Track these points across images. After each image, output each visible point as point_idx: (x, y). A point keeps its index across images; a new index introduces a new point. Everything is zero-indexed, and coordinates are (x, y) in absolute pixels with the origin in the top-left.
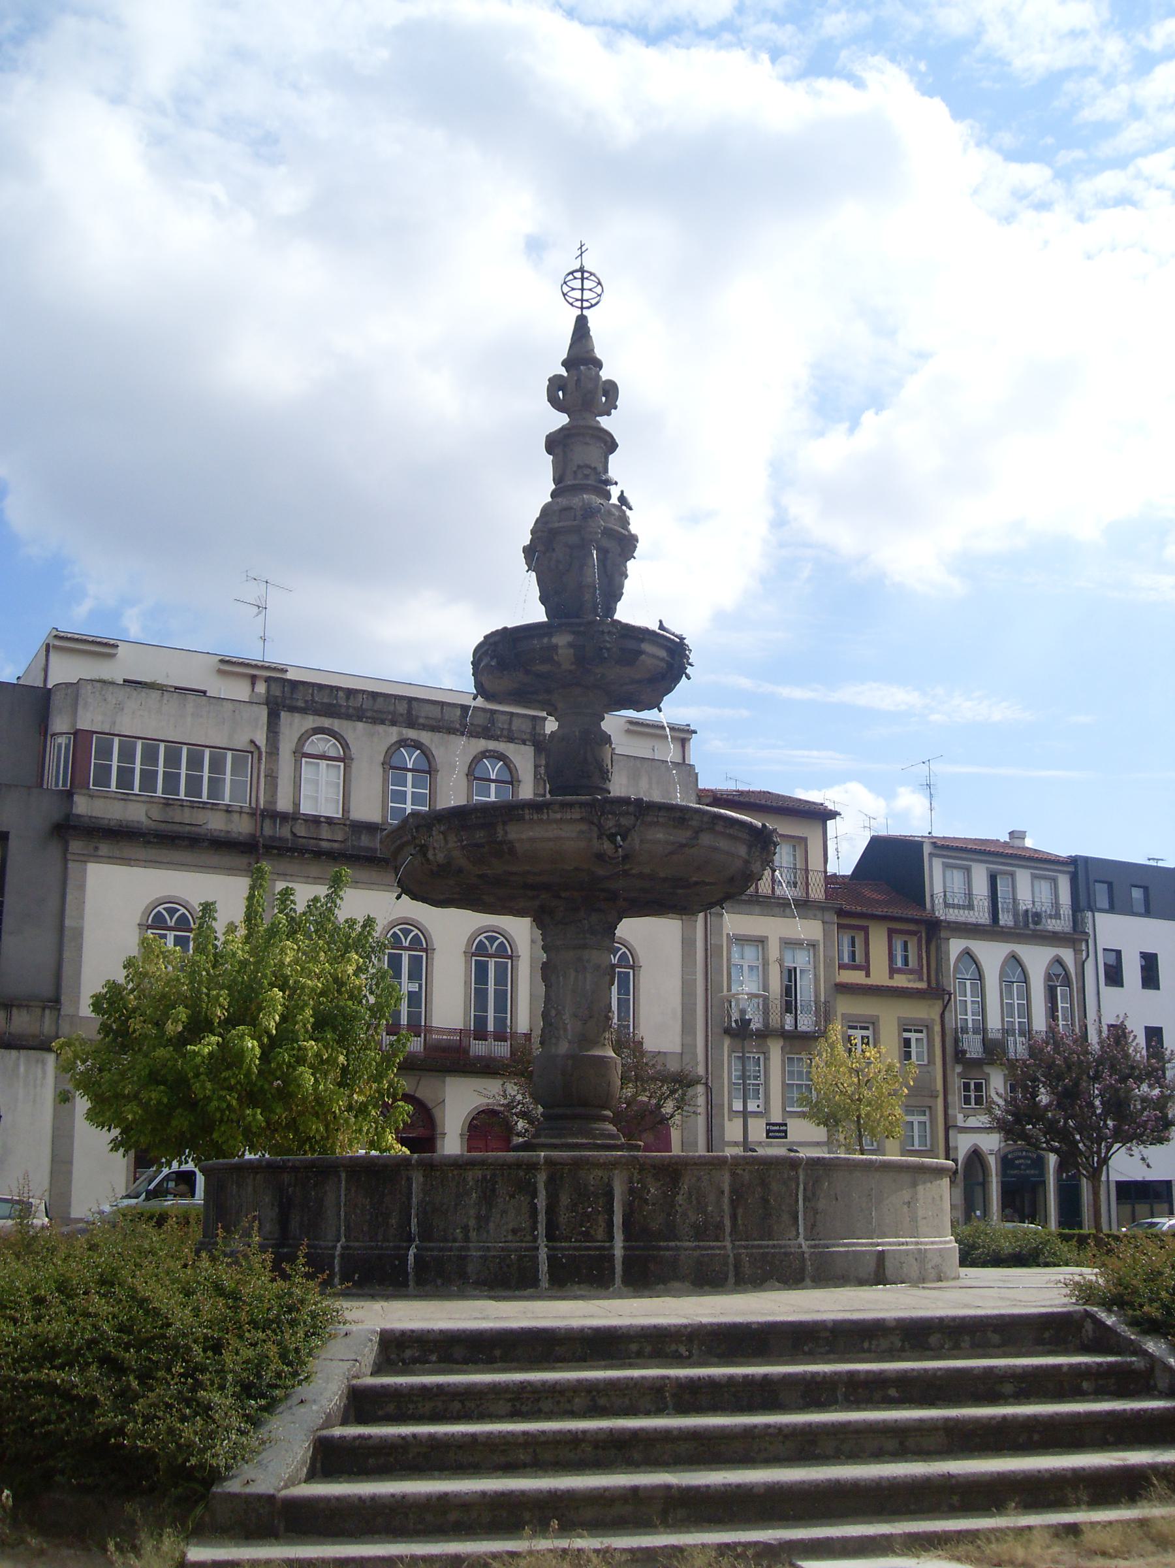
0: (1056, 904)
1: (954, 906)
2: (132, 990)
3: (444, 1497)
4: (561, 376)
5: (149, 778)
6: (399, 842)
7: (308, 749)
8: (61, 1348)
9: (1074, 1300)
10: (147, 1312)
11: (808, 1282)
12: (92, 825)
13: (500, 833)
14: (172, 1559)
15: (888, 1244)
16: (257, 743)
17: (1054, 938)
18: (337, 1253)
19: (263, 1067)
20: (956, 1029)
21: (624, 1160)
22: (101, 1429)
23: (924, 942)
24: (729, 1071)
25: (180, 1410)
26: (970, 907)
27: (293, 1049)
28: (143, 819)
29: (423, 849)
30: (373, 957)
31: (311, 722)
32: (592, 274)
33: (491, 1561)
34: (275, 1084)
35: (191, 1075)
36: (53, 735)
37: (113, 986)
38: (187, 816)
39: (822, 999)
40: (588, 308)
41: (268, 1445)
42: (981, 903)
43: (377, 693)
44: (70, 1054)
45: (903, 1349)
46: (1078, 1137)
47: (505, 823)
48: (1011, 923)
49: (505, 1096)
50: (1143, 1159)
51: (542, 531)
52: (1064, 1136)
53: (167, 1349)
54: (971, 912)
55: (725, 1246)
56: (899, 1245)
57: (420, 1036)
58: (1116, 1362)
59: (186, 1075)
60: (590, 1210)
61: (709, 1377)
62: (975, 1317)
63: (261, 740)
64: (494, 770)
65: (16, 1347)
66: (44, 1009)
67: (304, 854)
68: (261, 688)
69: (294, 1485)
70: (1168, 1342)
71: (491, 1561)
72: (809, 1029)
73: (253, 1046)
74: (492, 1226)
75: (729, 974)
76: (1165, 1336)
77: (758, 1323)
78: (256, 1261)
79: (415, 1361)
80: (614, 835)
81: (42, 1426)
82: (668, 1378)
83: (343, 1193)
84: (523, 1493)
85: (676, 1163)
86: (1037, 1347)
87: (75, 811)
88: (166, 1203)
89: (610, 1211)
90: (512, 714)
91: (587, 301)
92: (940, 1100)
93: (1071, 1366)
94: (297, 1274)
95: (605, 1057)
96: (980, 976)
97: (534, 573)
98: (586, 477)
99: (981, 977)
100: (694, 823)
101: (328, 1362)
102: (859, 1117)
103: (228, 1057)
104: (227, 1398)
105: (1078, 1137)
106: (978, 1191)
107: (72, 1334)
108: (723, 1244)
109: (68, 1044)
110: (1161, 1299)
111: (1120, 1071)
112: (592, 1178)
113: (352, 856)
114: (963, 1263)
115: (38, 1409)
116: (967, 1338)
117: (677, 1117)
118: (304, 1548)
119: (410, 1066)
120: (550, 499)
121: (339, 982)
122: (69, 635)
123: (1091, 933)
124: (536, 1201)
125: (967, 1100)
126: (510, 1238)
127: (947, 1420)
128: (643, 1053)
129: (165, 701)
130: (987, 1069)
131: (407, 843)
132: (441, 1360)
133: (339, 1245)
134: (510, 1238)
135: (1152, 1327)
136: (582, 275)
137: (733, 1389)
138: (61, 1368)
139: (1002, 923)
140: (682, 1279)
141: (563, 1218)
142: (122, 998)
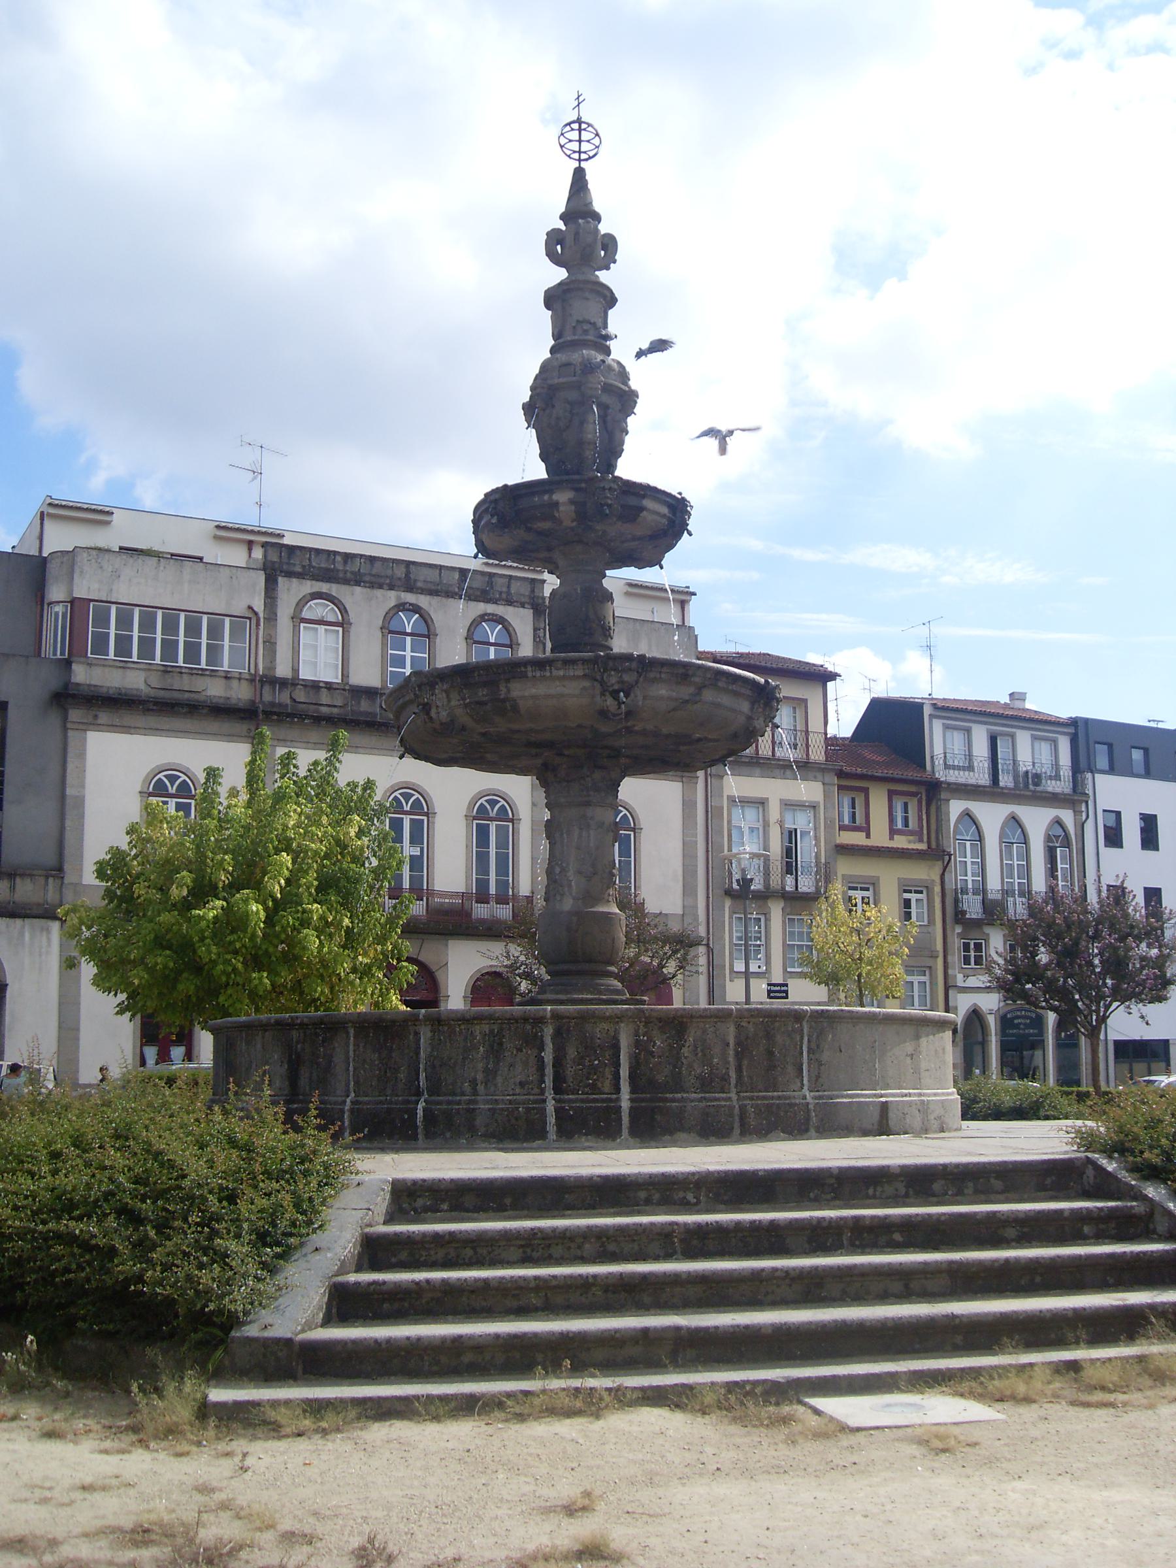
0: (1056, 765)
1: (954, 767)
2: (136, 857)
3: (458, 1340)
4: (559, 230)
5: (147, 646)
6: (401, 701)
7: (306, 614)
8: (78, 1200)
9: (1075, 1148)
10: (162, 1165)
11: (812, 1132)
12: (91, 694)
13: (503, 690)
14: (194, 1400)
15: (891, 1095)
16: (255, 609)
17: (1054, 800)
18: (347, 1108)
19: (268, 930)
20: (956, 889)
21: (630, 1014)
22: (121, 1278)
23: (924, 803)
24: (731, 931)
25: (198, 1258)
26: (970, 768)
27: (298, 912)
28: (142, 686)
29: (426, 708)
30: (376, 820)
31: (309, 587)
32: (589, 125)
33: (505, 1399)
34: (280, 948)
35: (196, 939)
36: (49, 604)
37: (117, 854)
38: (185, 683)
39: (823, 861)
40: (586, 160)
41: (284, 1291)
42: (981, 765)
43: (374, 557)
44: (76, 921)
45: (907, 1195)
46: (1077, 997)
47: (508, 681)
48: (1011, 785)
49: (508, 957)
50: (1142, 1017)
51: (543, 388)
52: (1064, 994)
53: (182, 1200)
54: (971, 773)
55: (730, 1098)
56: (902, 1096)
57: (422, 900)
58: (1117, 1207)
59: (191, 938)
60: (596, 1062)
61: (717, 1222)
62: (978, 1163)
63: (259, 606)
64: (493, 633)
65: (34, 1200)
66: (47, 877)
67: (304, 719)
68: (258, 553)
69: (310, 1329)
70: (1168, 1187)
71: (505, 1399)
72: (809, 891)
73: (258, 910)
74: (499, 1080)
75: (730, 836)
76: (1164, 1181)
77: (765, 1170)
78: (268, 1115)
79: (426, 1209)
80: (618, 692)
81: (63, 1275)
82: (677, 1224)
83: (351, 1047)
84: (535, 1335)
85: (682, 1017)
86: (1039, 1193)
87: (73, 680)
88: (174, 1067)
89: (617, 1065)
90: (510, 576)
91: (585, 152)
92: (940, 961)
93: (1072, 1210)
94: (309, 1126)
95: (609, 913)
96: (980, 836)
97: (534, 431)
98: (586, 332)
99: (981, 838)
100: (697, 679)
101: (341, 1212)
102: (859, 976)
103: (233, 921)
104: (243, 1246)
105: (1077, 997)
106: (978, 1049)
107: (89, 1186)
108: (728, 1095)
109: (74, 910)
110: (1161, 1146)
111: (1120, 931)
112: (600, 1030)
113: (352, 721)
114: (965, 1117)
115: (59, 1259)
116: (970, 1184)
117: (680, 977)
118: (323, 1389)
119: (413, 929)
120: (549, 355)
121: (342, 845)
122: (64, 503)
123: (1091, 793)
124: (543, 1054)
125: (967, 961)
126: (518, 1091)
127: (951, 1263)
128: (644, 915)
129: (162, 568)
130: (987, 930)
131: (411, 702)
132: (452, 1209)
133: (348, 1100)
134: (518, 1091)
135: (1152, 1173)
136: (580, 126)
137: (740, 1235)
138: (79, 1219)
139: (1001, 784)
140: (689, 1130)
141: (570, 1071)
142: (125, 865)
